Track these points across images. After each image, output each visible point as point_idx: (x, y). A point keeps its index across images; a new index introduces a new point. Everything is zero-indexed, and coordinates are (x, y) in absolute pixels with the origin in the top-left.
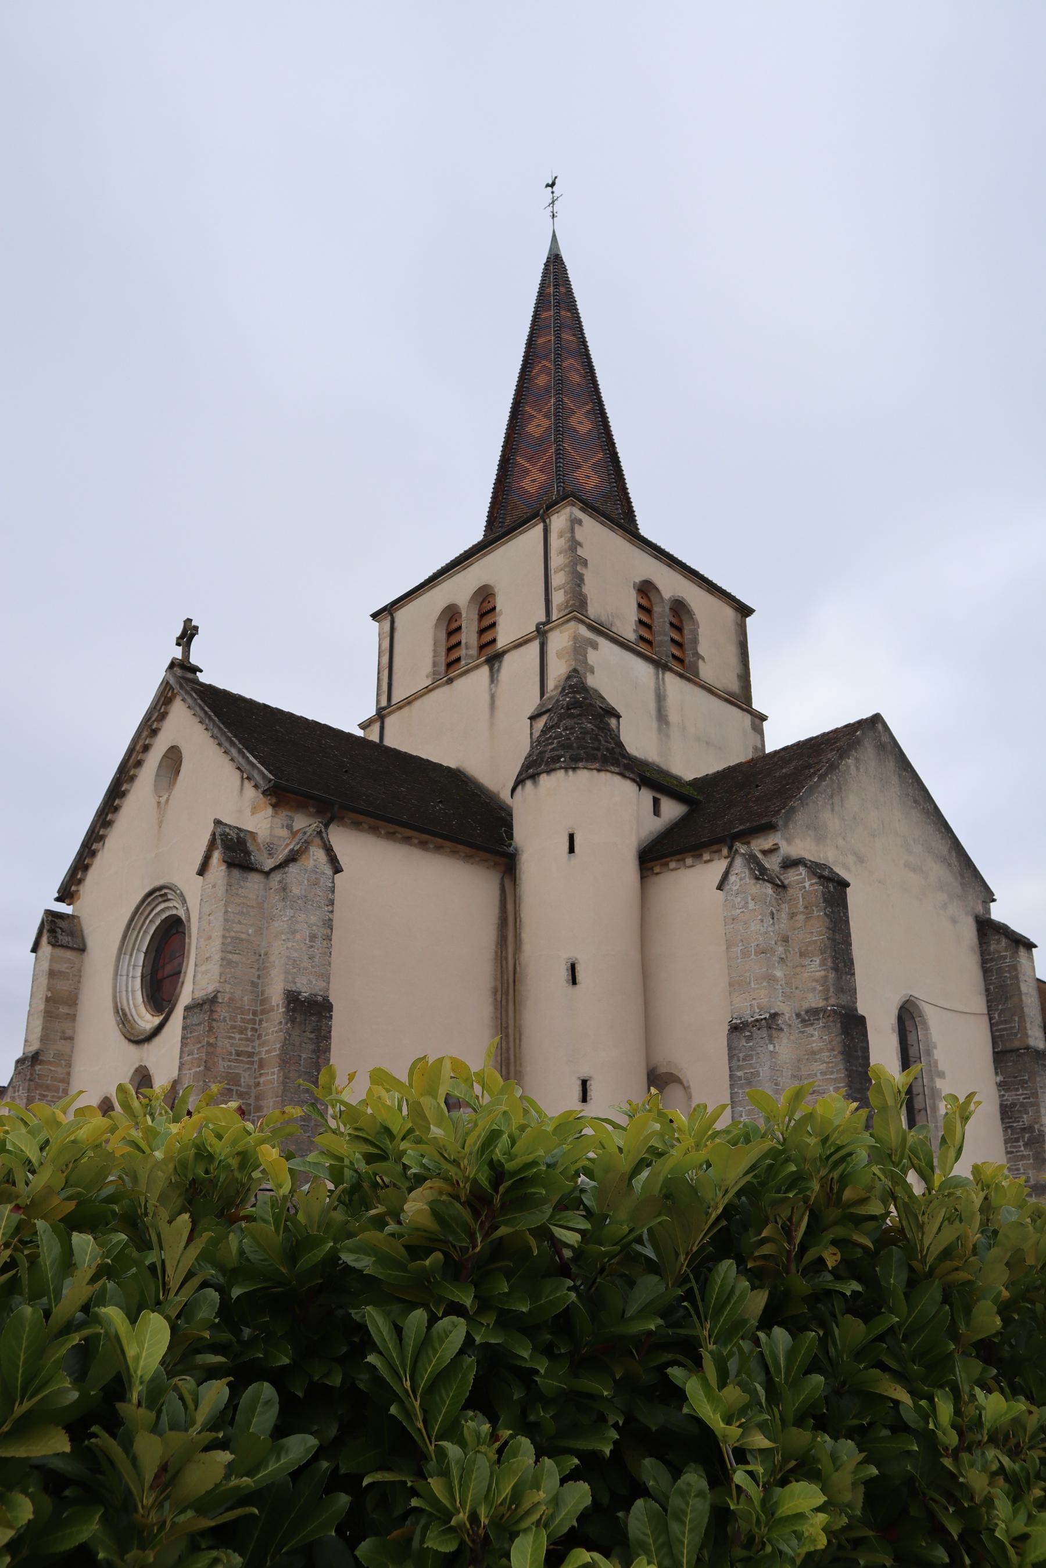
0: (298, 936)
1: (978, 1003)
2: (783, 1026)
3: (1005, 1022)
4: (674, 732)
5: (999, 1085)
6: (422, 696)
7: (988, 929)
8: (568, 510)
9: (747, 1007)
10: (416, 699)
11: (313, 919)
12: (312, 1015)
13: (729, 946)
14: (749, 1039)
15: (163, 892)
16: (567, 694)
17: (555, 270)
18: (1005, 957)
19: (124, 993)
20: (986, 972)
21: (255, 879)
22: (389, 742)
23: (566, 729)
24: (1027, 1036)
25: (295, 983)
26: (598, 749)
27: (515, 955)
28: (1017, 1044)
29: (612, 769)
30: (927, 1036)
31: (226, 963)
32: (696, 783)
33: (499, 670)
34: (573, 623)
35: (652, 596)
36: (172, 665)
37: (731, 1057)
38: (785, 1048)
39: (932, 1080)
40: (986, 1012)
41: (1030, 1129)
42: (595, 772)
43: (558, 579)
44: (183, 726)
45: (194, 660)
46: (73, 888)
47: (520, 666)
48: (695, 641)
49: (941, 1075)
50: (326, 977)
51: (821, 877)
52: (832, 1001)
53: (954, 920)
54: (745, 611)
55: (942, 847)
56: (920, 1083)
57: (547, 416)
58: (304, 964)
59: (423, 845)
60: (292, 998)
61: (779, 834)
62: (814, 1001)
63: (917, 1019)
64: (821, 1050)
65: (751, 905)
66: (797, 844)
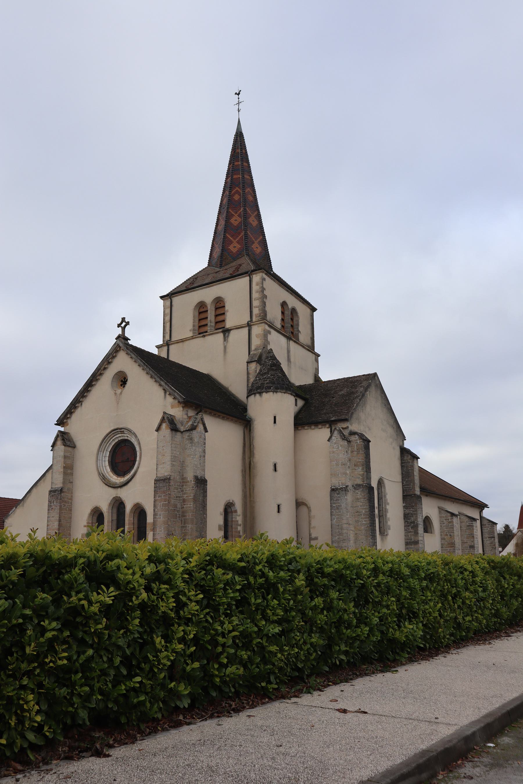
0: (197, 456)
1: (399, 478)
3: (408, 485)
4: (292, 365)
5: (404, 507)
6: (189, 340)
7: (405, 453)
8: (261, 274)
9: (337, 482)
10: (186, 340)
13: (331, 461)
14: (338, 494)
15: (122, 430)
16: (270, 360)
17: (239, 140)
18: (409, 462)
19: (101, 467)
20: (402, 467)
21: (179, 434)
22: (172, 358)
23: (272, 375)
24: (415, 490)
26: (284, 384)
27: (250, 458)
28: (411, 493)
29: (289, 392)
30: (385, 490)
31: (173, 465)
32: (300, 387)
33: (228, 336)
34: (263, 324)
36: (118, 338)
37: (331, 500)
38: (349, 497)
39: (386, 506)
41: (414, 522)
43: (256, 303)
44: (124, 363)
45: (127, 335)
46: (65, 421)
47: (238, 338)
48: (298, 325)
49: (388, 504)
50: (204, 470)
51: (364, 440)
52: (365, 482)
53: (394, 448)
54: (314, 309)
55: (392, 422)
57: (239, 216)
58: (199, 466)
59: (223, 418)
60: (196, 478)
61: (349, 423)
62: (359, 482)
64: (361, 498)
65: (340, 448)
66: (354, 427)
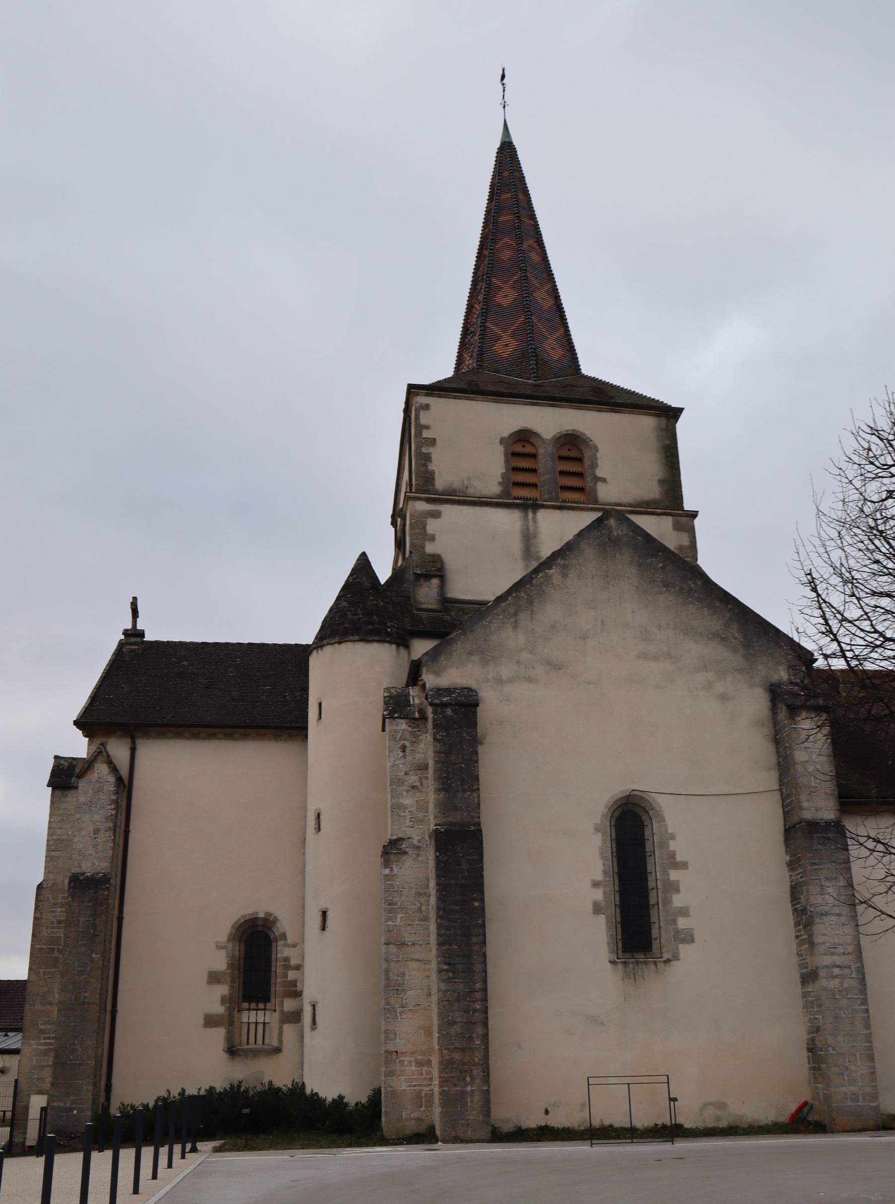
0: (83, 832)
2: (407, 850)
11: (96, 817)
12: (90, 889)
17: (507, 154)
25: (80, 867)
35: (534, 441)
40: (776, 787)
42: (337, 645)
45: (139, 627)
56: (654, 877)
58: (89, 852)
63: (651, 812)
